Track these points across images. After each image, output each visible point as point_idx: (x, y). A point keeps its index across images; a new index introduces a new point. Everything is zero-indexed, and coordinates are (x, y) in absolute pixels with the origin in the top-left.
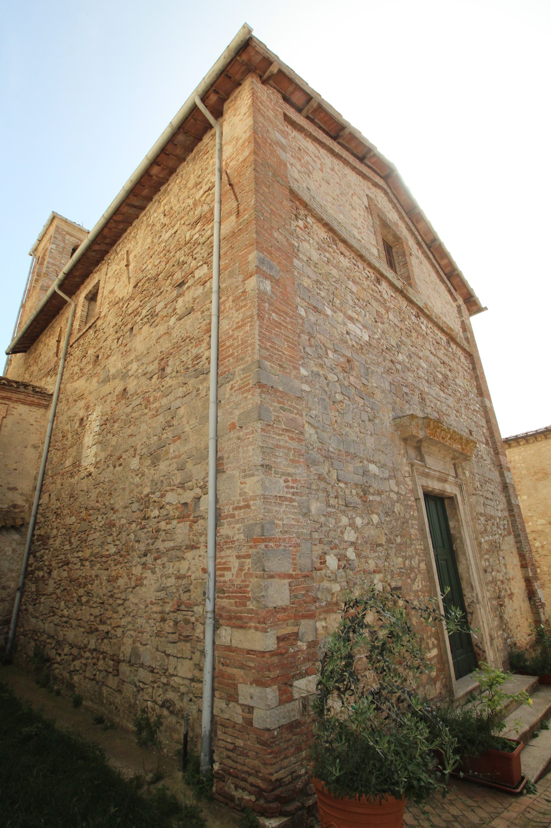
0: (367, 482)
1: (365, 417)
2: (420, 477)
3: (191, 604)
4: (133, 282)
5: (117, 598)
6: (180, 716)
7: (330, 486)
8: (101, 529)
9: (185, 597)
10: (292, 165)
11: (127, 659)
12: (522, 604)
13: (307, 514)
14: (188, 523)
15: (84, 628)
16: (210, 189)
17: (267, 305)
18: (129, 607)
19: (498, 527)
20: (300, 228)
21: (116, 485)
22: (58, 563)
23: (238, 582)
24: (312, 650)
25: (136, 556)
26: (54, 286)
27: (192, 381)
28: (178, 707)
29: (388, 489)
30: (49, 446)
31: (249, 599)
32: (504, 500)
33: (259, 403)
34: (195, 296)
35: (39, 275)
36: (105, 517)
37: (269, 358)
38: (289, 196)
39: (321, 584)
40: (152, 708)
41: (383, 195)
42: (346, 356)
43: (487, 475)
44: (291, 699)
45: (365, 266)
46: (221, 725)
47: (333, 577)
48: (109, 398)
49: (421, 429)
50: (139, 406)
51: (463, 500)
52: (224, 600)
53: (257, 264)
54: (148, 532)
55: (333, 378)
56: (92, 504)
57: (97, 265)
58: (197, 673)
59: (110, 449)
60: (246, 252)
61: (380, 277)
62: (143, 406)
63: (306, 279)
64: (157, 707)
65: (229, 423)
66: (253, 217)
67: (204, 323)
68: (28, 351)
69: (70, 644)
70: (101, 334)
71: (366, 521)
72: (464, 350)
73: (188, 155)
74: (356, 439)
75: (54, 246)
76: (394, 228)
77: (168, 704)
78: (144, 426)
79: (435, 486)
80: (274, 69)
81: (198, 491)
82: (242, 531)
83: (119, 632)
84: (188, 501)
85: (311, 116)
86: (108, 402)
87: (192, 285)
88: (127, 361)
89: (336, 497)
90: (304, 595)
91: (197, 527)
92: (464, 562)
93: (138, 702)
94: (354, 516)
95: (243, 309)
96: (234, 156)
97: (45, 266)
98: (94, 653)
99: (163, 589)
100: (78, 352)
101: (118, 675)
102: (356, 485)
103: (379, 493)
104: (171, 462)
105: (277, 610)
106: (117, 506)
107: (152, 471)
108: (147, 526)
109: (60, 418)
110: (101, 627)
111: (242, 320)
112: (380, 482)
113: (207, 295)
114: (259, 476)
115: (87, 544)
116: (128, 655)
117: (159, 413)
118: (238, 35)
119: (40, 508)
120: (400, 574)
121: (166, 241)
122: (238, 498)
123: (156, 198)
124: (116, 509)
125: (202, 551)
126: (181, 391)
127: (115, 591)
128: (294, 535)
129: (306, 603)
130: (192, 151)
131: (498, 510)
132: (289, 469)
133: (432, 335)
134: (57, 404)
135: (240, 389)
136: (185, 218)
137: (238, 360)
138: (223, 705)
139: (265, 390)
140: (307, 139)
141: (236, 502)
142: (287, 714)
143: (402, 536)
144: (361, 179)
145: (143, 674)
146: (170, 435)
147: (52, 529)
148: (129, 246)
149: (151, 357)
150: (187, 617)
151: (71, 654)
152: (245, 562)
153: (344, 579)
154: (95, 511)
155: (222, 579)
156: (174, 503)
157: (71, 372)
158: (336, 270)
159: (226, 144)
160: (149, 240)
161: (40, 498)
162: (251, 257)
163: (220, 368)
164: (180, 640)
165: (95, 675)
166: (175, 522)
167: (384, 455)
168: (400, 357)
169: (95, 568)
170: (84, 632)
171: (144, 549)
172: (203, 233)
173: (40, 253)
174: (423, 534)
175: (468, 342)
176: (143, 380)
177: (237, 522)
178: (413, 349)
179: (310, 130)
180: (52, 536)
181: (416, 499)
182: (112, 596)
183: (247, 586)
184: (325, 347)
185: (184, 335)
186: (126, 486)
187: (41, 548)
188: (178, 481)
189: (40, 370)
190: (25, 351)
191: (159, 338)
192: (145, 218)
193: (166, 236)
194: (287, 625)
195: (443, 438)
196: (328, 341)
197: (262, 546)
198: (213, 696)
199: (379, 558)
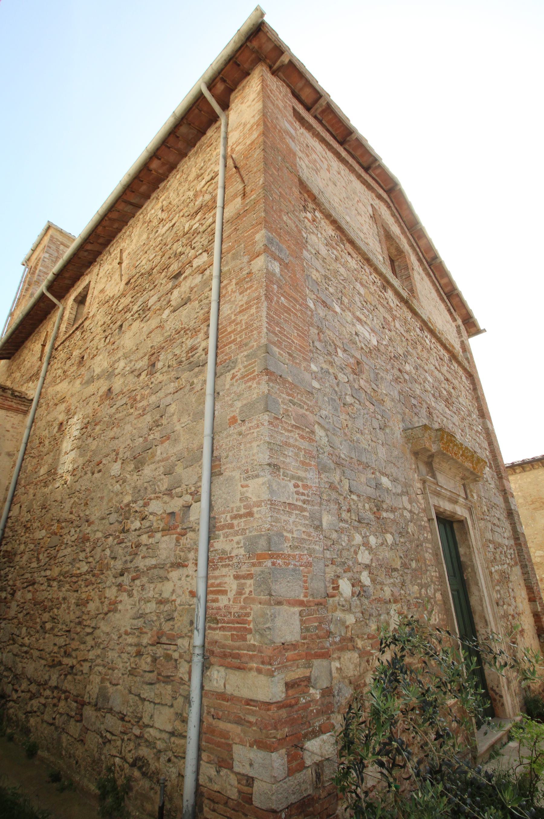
0: (380, 496)
1: (376, 425)
2: (432, 495)
3: (174, 636)
4: (125, 279)
5: (86, 626)
6: (155, 780)
7: (342, 497)
8: (73, 544)
9: (166, 627)
10: (300, 158)
11: (93, 701)
12: (532, 642)
13: (318, 528)
14: (175, 536)
15: (46, 660)
16: (212, 179)
17: (275, 287)
18: (99, 637)
19: (506, 556)
20: (309, 220)
21: (93, 494)
22: (23, 583)
23: (236, 610)
24: (327, 700)
25: (111, 575)
26: (42, 288)
27: (185, 375)
28: (152, 768)
29: (401, 506)
30: (24, 453)
31: (250, 631)
32: (509, 527)
33: (266, 391)
34: (192, 286)
35: (29, 285)
36: (78, 530)
37: (278, 344)
38: (298, 184)
39: (334, 614)
40: (120, 767)
41: (386, 209)
42: (356, 358)
43: (492, 499)
44: (302, 767)
45: (372, 271)
46: (209, 799)
47: (347, 606)
48: (92, 400)
49: (434, 442)
50: (125, 406)
51: (473, 524)
52: (217, 632)
53: (266, 242)
54: (126, 547)
55: (343, 378)
56: (65, 515)
57: (89, 267)
58: (178, 725)
59: (89, 454)
60: (252, 232)
61: (387, 284)
62: (129, 406)
63: (314, 272)
64: (126, 766)
65: (228, 417)
66: (262, 196)
67: (202, 311)
68: (12, 358)
69: (29, 680)
70: (88, 334)
71: (380, 541)
72: (465, 369)
73: (190, 150)
74: (367, 447)
75: (47, 255)
76: (397, 241)
77: (140, 763)
78: (128, 428)
79: (447, 506)
80: (285, 59)
81: (188, 498)
82: (242, 545)
83: (86, 667)
84: (176, 510)
85: (319, 117)
86: (91, 403)
87: (190, 275)
88: (113, 359)
89: (349, 511)
90: (317, 628)
91: (185, 541)
92: (477, 593)
93: (103, 757)
94: (368, 534)
95: (248, 291)
96: (240, 141)
97: (36, 275)
98: (56, 692)
99: (141, 616)
100: (62, 355)
101: (80, 721)
102: (369, 498)
103: (393, 510)
104: (157, 465)
105: (286, 647)
106: (92, 518)
107: (135, 477)
108: (125, 540)
109: (39, 424)
110: (65, 661)
111: (246, 303)
112: (393, 497)
113: (207, 283)
114: (266, 477)
115: (57, 561)
116: (95, 696)
117: (146, 412)
118: (249, 18)
119: (9, 521)
120: (417, 605)
121: (163, 235)
122: (238, 504)
123: (154, 195)
124: (91, 520)
125: (190, 570)
126: (172, 387)
127: (84, 617)
128: (306, 552)
129: (319, 637)
130: (194, 146)
131: (504, 538)
132: (299, 471)
133: (435, 350)
134: (36, 410)
135: (243, 377)
136: (184, 211)
137: (241, 346)
138: (213, 772)
139: (273, 378)
140: (315, 139)
141: (235, 509)
142: (298, 787)
143: (417, 561)
144: (366, 189)
145: (111, 722)
146: (157, 435)
147: (19, 544)
148: (123, 245)
149: (140, 353)
150: (169, 652)
151: (29, 691)
152: (246, 583)
153: (359, 609)
154: (67, 524)
155: (215, 605)
156: (159, 513)
157: (54, 375)
158: (344, 269)
159: (232, 130)
160: (145, 236)
161: (10, 510)
162: (258, 237)
163: (220, 356)
164: (158, 681)
165: (54, 719)
166: (158, 535)
167: (396, 469)
168: (408, 368)
169: (64, 589)
170: (45, 666)
171: (120, 567)
172: (203, 222)
173: (32, 263)
174: (437, 559)
175: (469, 363)
176: (131, 378)
177: (236, 534)
178: (419, 361)
179: (318, 130)
180: (19, 552)
181: (429, 520)
182: (80, 623)
183: (248, 615)
184: (335, 345)
185: (178, 326)
186: (105, 494)
187: (6, 565)
188: (165, 487)
189: (23, 376)
190: (9, 358)
191: (151, 332)
192: (141, 216)
193: (162, 230)
194: (298, 667)
195: (456, 454)
196: (338, 339)
197: (269, 563)
198: (199, 758)
199: (394, 585)
